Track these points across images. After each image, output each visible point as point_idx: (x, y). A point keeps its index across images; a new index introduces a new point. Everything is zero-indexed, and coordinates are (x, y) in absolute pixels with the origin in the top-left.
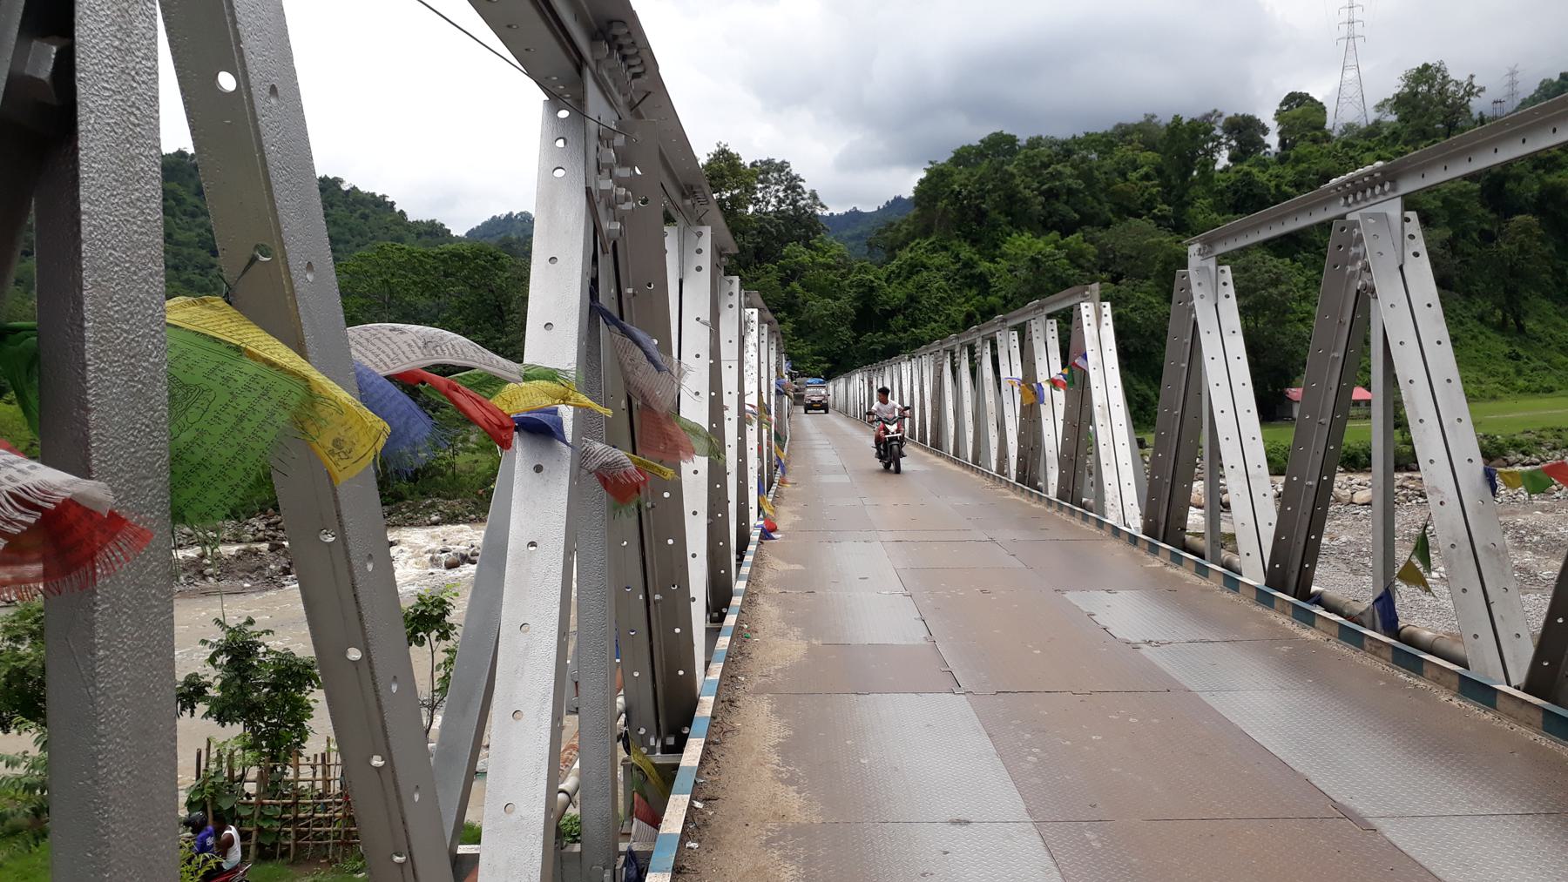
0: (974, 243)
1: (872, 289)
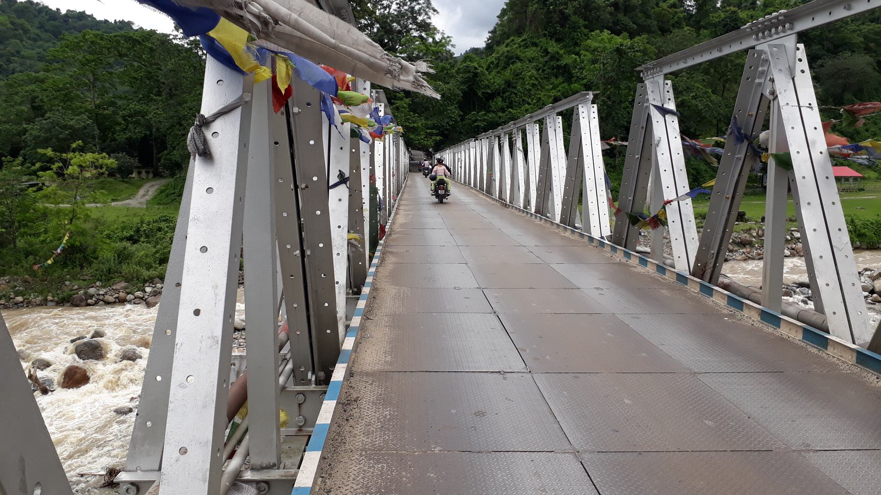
0: (558, 40)
1: (476, 75)
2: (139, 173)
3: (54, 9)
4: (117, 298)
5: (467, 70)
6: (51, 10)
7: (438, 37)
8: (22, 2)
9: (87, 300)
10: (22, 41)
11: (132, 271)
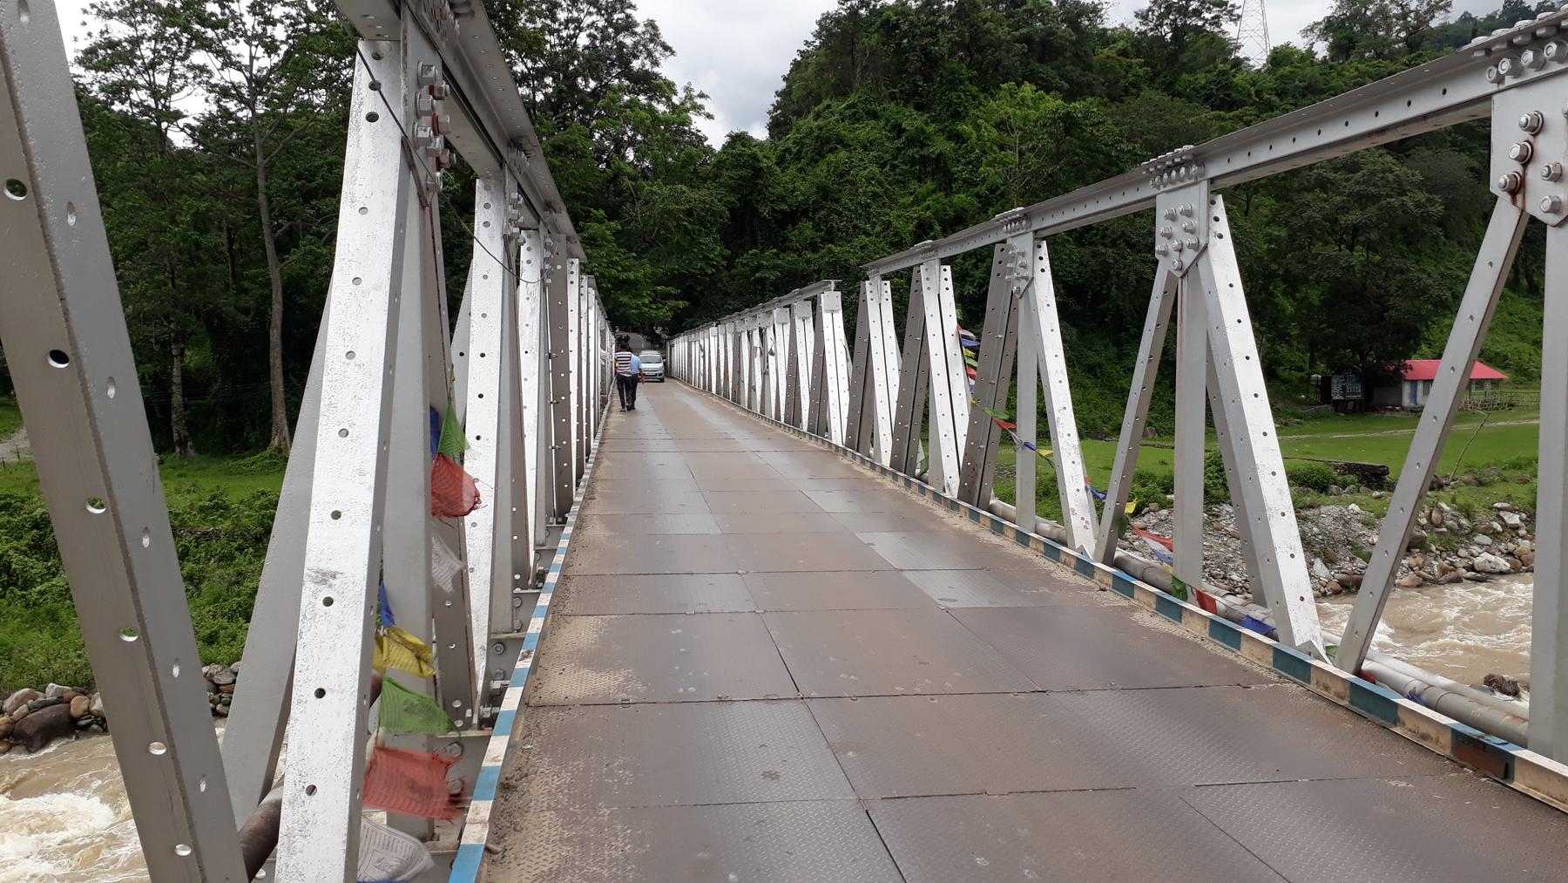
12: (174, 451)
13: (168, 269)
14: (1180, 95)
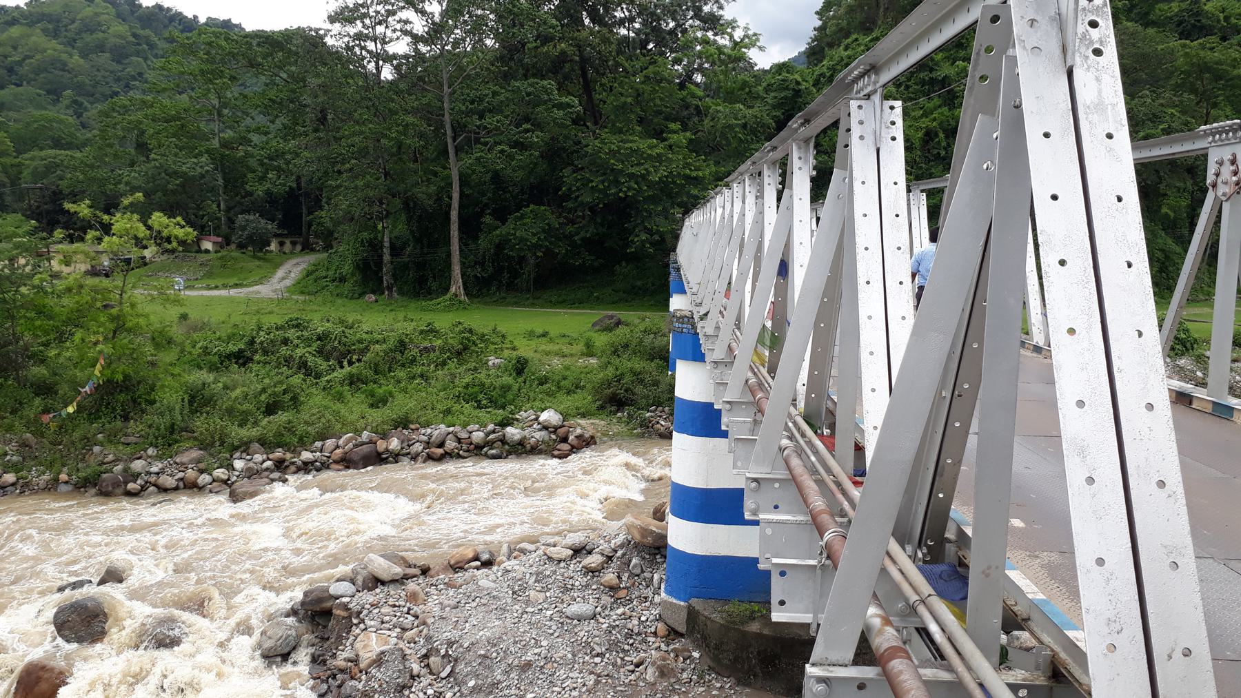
1: (797, 93)
2: (282, 244)
3: (190, 16)
4: (182, 479)
5: (783, 85)
6: (187, 17)
7: (738, 35)
8: (148, 8)
9: (126, 483)
10: (146, 59)
11: (212, 428)
12: (383, 293)
13: (382, 166)
14: (1153, 24)
